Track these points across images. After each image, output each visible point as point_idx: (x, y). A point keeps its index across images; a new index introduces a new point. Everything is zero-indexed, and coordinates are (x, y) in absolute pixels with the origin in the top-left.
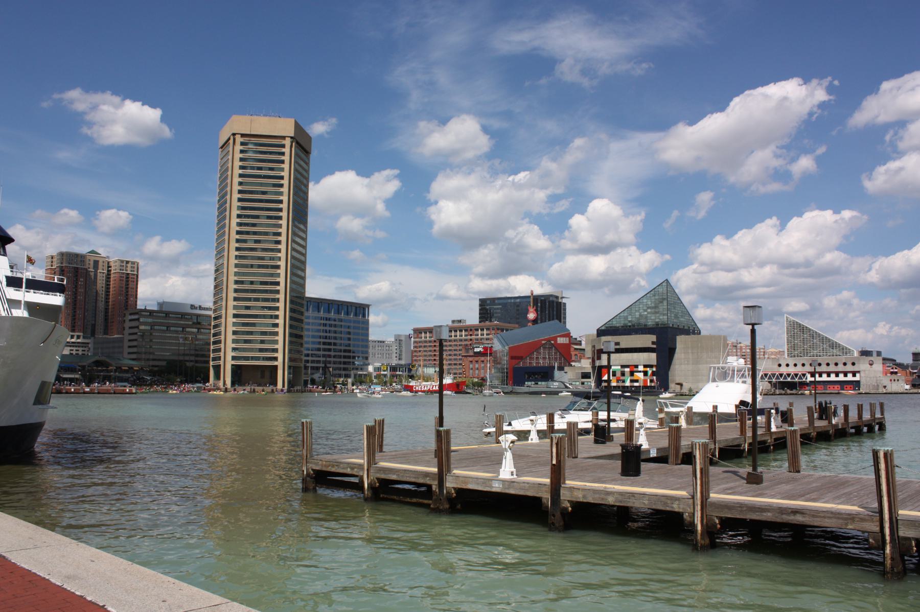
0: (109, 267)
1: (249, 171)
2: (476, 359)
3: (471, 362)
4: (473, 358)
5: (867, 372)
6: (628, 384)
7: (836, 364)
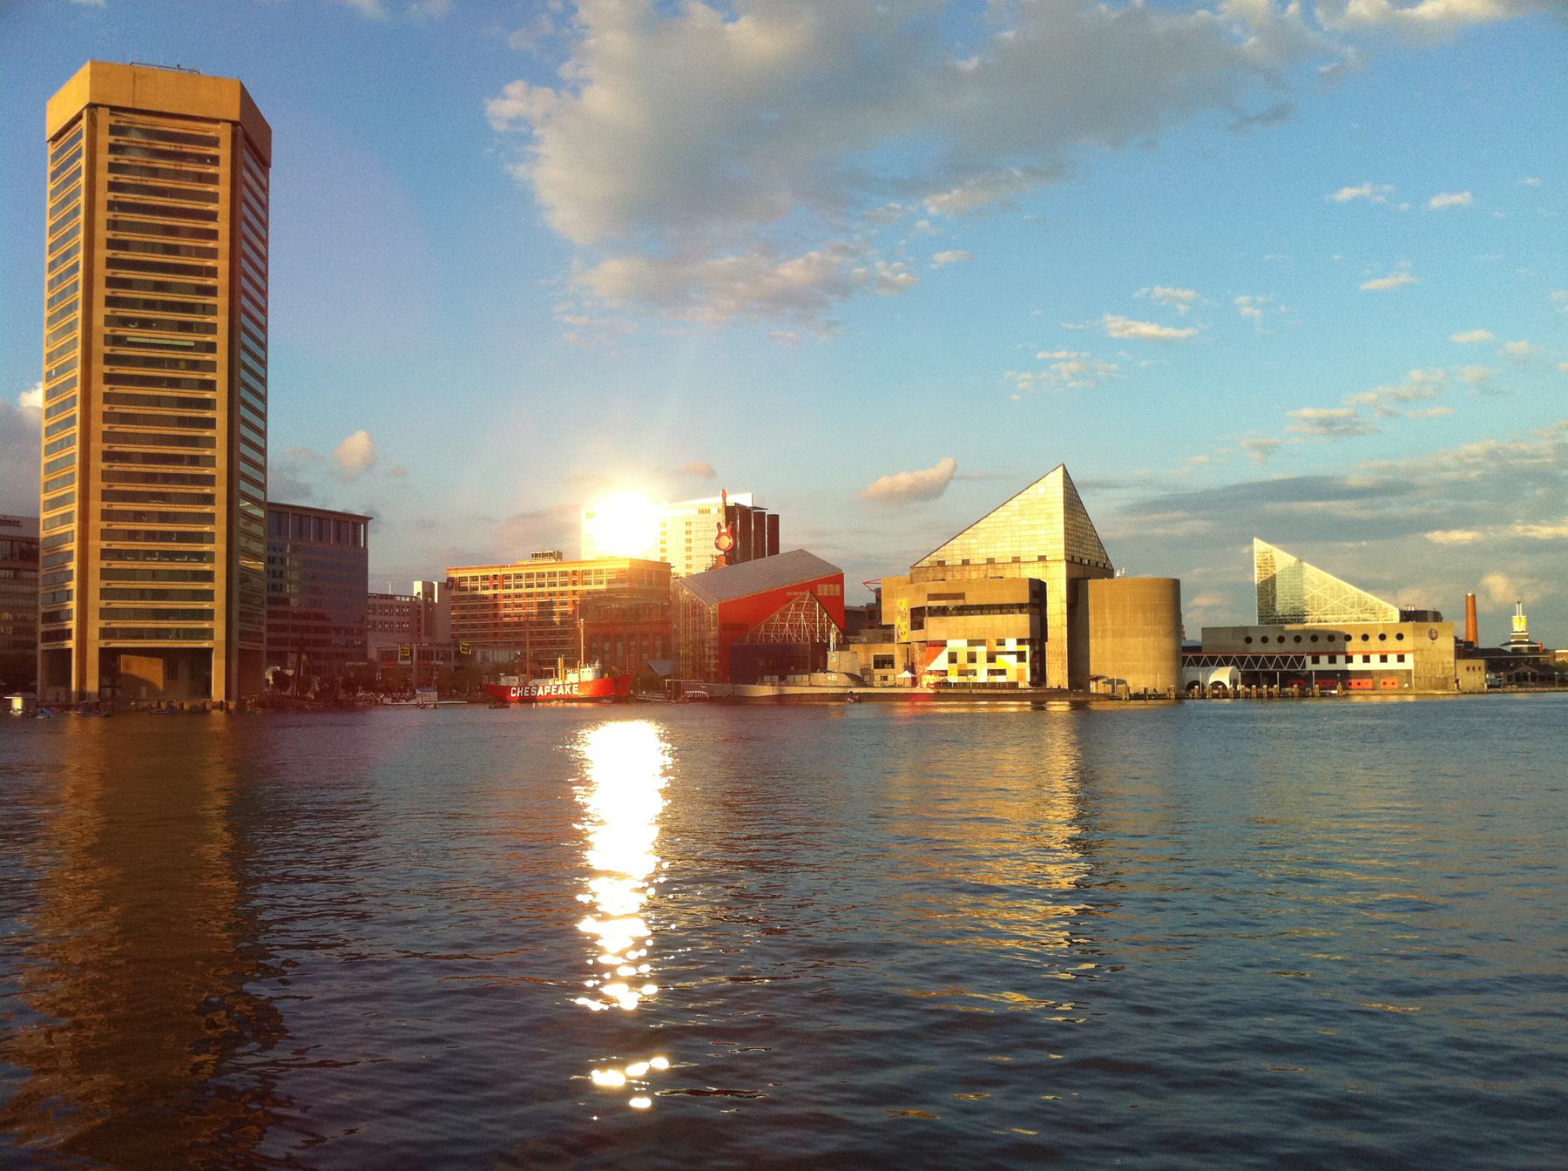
5: (1425, 653)
6: (982, 677)
7: (1365, 638)
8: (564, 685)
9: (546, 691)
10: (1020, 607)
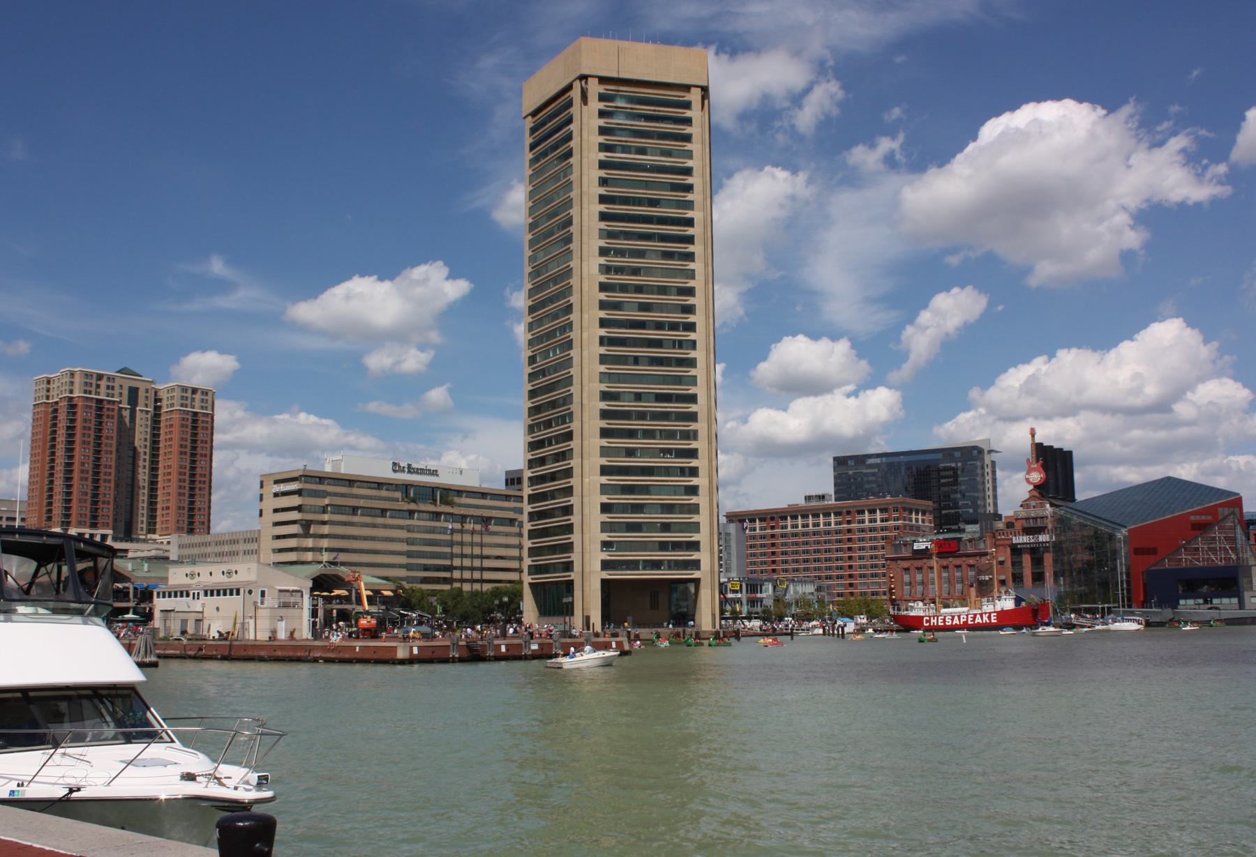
0: (157, 400)
1: (619, 156)
2: (918, 563)
3: (907, 569)
4: (912, 562)
8: (981, 615)
9: (962, 620)
10: (472, 573)
